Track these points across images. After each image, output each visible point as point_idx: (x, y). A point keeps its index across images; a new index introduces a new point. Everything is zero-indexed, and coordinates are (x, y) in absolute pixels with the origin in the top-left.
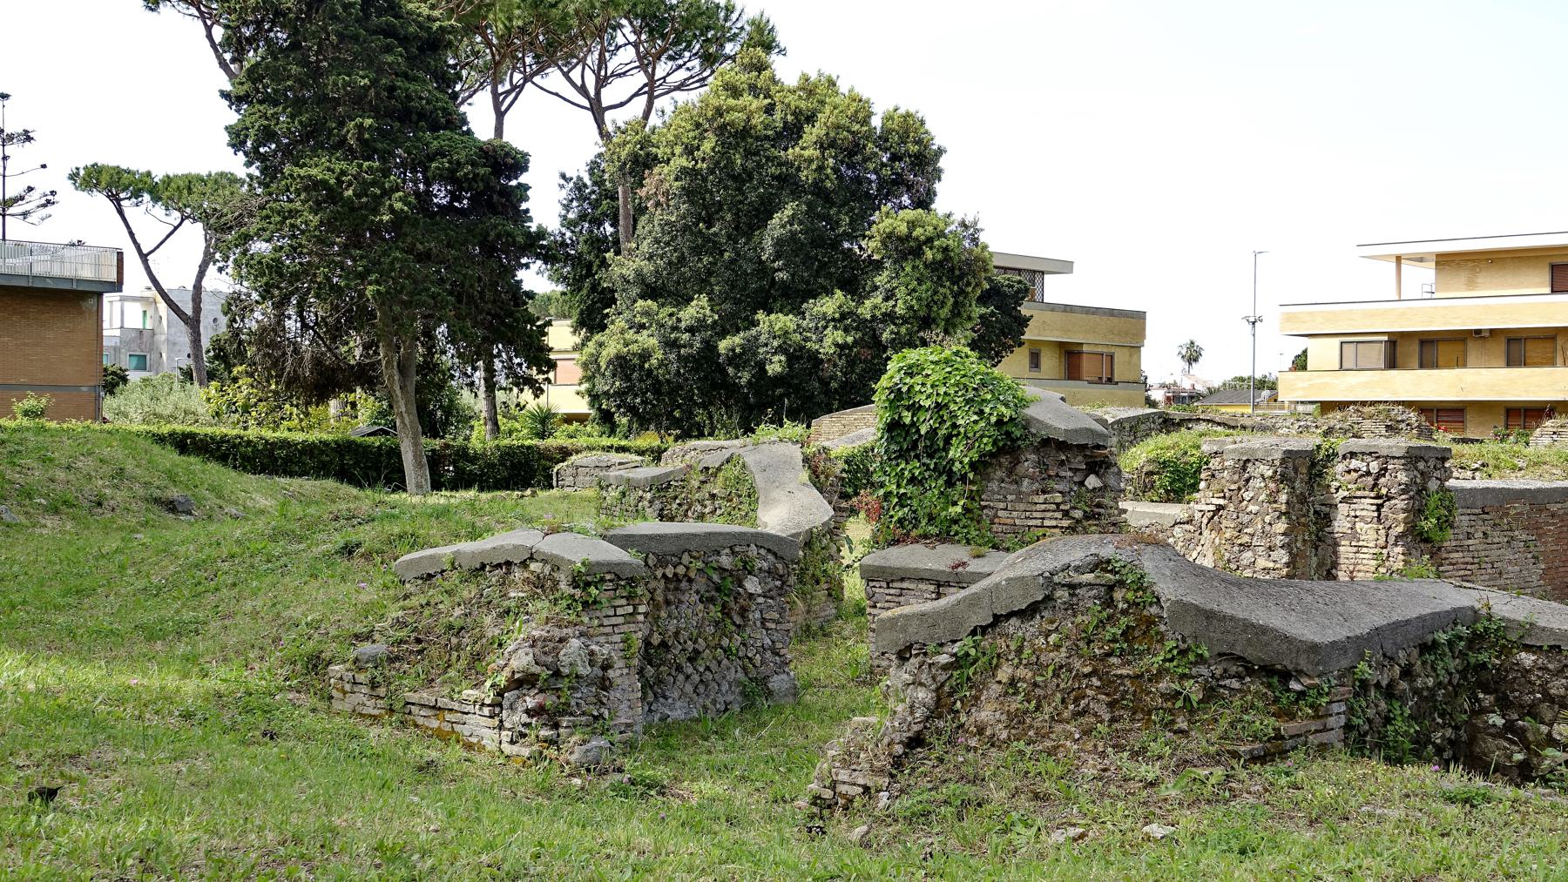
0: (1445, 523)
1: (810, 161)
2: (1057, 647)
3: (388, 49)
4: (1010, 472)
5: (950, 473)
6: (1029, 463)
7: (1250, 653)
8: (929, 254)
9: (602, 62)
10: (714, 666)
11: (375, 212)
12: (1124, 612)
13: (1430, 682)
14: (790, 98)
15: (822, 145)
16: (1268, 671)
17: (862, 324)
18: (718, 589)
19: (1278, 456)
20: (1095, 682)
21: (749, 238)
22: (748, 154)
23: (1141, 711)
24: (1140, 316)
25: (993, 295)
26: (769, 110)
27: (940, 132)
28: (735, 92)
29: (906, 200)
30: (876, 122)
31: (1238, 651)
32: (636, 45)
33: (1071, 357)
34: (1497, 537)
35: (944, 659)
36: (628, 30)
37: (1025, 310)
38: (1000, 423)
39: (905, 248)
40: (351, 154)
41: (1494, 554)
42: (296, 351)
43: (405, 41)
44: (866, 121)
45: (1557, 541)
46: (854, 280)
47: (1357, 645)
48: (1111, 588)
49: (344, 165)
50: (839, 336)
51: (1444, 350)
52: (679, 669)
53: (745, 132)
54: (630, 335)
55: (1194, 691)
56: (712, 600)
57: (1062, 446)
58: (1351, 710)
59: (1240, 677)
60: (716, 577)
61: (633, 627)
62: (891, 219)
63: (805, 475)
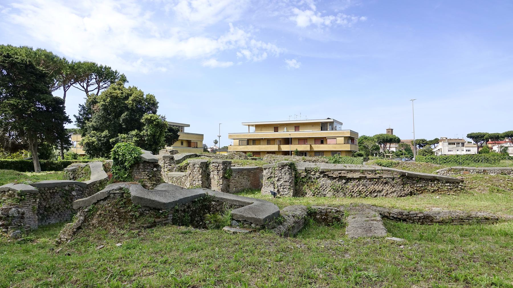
0: (230, 175)
1: (130, 104)
2: (110, 207)
3: (32, 76)
4: (138, 168)
5: (126, 168)
6: (141, 166)
7: (151, 206)
8: (155, 123)
9: (88, 82)
10: (63, 211)
11: (27, 111)
12: (125, 199)
13: (194, 208)
14: (127, 91)
15: (133, 100)
16: (155, 209)
17: (141, 137)
18: (65, 194)
19: (200, 163)
20: (117, 213)
21: (118, 118)
22: (117, 102)
23: (125, 219)
24: (203, 135)
25: (171, 130)
26: (122, 93)
27: (158, 99)
28: (115, 89)
29: (151, 112)
30: (145, 96)
31: (148, 205)
32: (96, 79)
33: (189, 143)
34: (241, 177)
35: (86, 210)
36: (94, 76)
37: (178, 134)
38: (135, 158)
39: (150, 121)
40: (20, 98)
41: (240, 180)
42: (7, 141)
43: (36, 75)
44: (142, 96)
45: (253, 177)
46: (140, 127)
47: (175, 203)
48: (123, 193)
49: (19, 101)
50: (136, 139)
51: (271, 142)
52: (54, 212)
53: (117, 97)
54: (90, 138)
55: (137, 214)
56: (64, 197)
57: (148, 162)
58: (174, 215)
59: (149, 211)
60: (64, 192)
61: (35, 204)
62: (147, 116)
63: (102, 169)
